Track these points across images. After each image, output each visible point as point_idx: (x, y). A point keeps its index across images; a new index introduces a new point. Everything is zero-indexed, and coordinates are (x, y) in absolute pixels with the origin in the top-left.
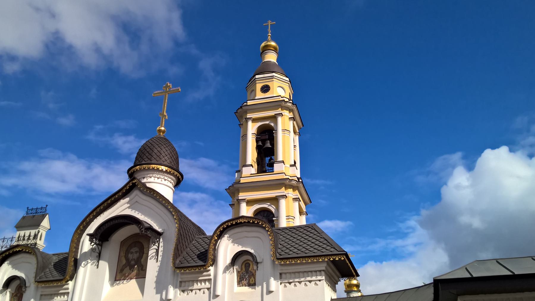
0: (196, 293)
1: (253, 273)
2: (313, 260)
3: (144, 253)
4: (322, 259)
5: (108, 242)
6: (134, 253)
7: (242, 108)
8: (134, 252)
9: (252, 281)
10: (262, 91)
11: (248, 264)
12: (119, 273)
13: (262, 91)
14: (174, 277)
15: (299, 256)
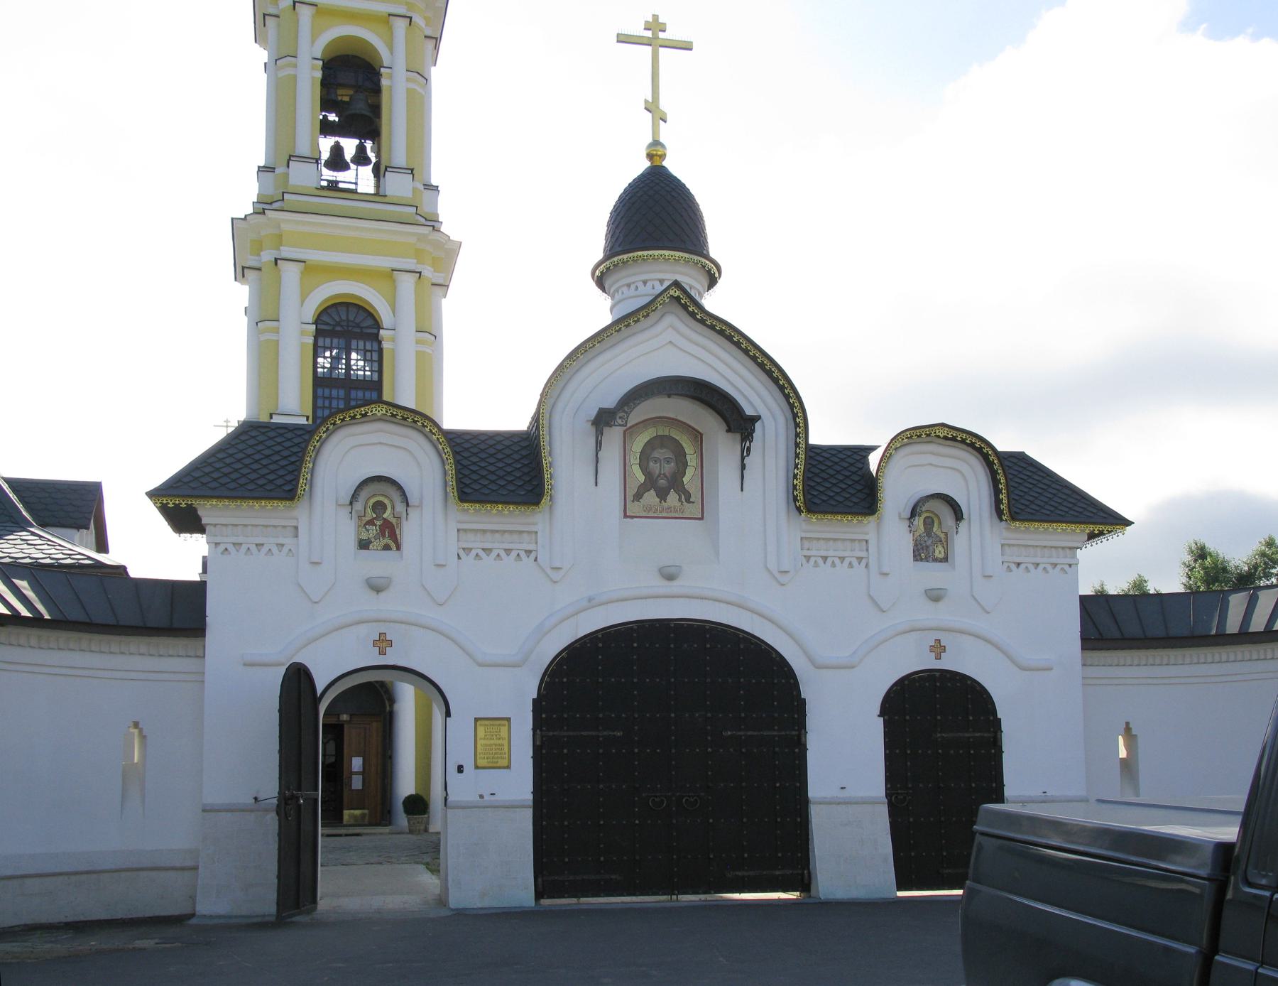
0: (1092, 546)
1: (941, 538)
2: (314, 447)
6: (662, 462)
8: (662, 458)
9: (940, 553)
11: (930, 520)
12: (633, 501)
14: (446, 520)
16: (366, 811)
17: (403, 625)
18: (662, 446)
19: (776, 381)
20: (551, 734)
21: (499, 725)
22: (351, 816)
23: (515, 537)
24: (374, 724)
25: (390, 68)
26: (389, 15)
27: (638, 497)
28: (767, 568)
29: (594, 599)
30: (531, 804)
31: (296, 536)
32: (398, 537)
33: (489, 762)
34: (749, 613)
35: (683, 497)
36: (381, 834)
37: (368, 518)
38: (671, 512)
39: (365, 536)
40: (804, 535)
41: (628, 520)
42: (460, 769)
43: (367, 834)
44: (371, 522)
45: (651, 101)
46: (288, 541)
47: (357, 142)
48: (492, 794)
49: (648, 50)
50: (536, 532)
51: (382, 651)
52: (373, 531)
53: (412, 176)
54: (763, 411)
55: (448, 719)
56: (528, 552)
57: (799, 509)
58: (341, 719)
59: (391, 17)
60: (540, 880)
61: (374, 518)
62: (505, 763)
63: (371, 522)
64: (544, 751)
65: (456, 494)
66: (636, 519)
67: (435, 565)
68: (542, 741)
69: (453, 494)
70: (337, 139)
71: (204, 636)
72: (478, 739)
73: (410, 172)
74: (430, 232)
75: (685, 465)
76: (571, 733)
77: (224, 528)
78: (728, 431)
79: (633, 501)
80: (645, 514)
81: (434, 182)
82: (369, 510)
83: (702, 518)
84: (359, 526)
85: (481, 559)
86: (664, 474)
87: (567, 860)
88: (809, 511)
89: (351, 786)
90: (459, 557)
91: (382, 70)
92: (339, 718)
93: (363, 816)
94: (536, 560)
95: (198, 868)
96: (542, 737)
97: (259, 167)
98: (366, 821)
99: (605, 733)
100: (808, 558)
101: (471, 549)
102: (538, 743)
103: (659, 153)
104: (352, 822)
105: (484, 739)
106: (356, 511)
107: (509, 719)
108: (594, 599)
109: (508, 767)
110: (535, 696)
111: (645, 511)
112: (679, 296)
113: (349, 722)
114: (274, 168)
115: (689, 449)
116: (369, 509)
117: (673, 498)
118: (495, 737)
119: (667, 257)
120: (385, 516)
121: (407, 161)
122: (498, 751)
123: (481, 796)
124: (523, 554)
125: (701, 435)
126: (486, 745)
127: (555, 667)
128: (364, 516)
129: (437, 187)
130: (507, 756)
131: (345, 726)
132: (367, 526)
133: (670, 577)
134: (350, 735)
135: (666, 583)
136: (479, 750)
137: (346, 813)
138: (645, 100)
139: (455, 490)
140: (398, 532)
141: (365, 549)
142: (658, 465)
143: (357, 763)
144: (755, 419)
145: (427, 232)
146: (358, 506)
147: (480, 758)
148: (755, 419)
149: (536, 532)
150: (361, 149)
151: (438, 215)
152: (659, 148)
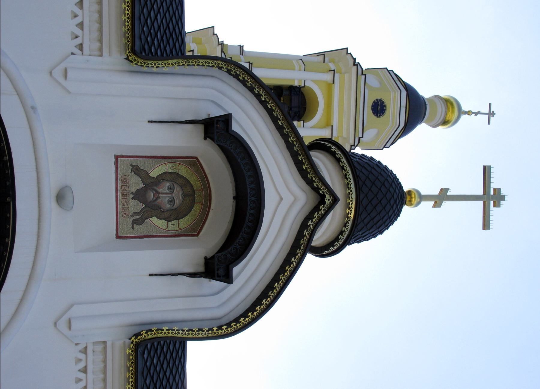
3: (168, 221)
4: (148, 67)
5: (203, 139)
6: (170, 195)
7: (354, 65)
8: (174, 195)
10: (379, 100)
13: (379, 100)
15: (327, 225)
18: (184, 195)
19: (252, 309)
23: (96, 35)
25: (304, 127)
26: (332, 126)
27: (136, 170)
28: (72, 306)
34: (23, 288)
35: (138, 217)
38: (123, 204)
40: (109, 344)
41: (113, 160)
45: (448, 194)
49: (480, 192)
50: (101, 55)
54: (237, 283)
56: (81, 47)
57: (136, 335)
59: (331, 127)
66: (114, 167)
75: (168, 219)
78: (206, 258)
79: (132, 165)
80: (120, 177)
83: (118, 237)
86: (159, 197)
88: (137, 346)
91: (302, 122)
94: (73, 54)
97: (243, 46)
100: (85, 351)
103: (413, 200)
111: (122, 177)
112: (325, 203)
114: (243, 55)
115: (184, 223)
117: (136, 206)
119: (350, 196)
124: (78, 41)
125: (197, 235)
133: (60, 198)
135: (54, 194)
138: (448, 189)
142: (168, 191)
144: (228, 278)
148: (228, 278)
149: (101, 55)
152: (418, 199)
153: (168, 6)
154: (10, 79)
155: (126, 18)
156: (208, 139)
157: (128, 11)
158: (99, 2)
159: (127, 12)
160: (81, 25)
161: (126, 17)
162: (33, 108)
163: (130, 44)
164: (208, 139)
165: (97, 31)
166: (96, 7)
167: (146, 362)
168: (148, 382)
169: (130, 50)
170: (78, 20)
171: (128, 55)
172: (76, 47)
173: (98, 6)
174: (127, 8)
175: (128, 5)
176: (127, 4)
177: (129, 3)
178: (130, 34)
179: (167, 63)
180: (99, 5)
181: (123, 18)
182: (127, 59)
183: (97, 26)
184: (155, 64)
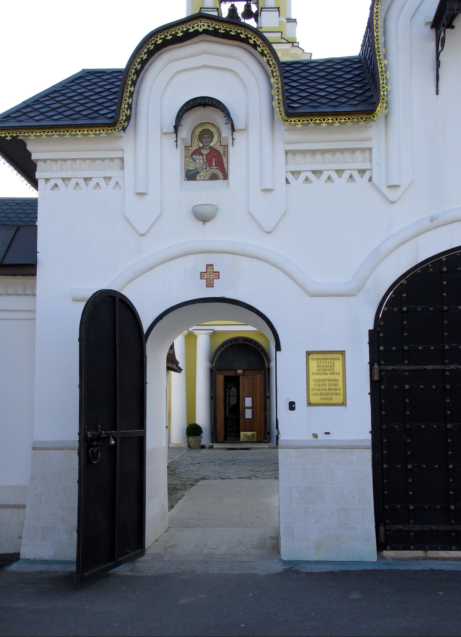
5: (453, 29)
16: (255, 433)
17: (230, 256)
20: (390, 368)
21: (333, 359)
22: (245, 436)
23: (347, 156)
24: (259, 376)
29: (436, 218)
30: (370, 444)
31: (123, 168)
32: (226, 166)
33: (323, 399)
36: (263, 448)
37: (194, 148)
39: (192, 167)
42: (292, 406)
43: (254, 448)
44: (198, 152)
46: (114, 173)
47: (245, 3)
48: (326, 433)
50: (370, 149)
51: (210, 284)
52: (200, 160)
53: (278, 12)
55: (278, 352)
56: (362, 172)
58: (238, 373)
60: (382, 529)
61: (200, 148)
62: (340, 399)
63: (198, 152)
64: (383, 387)
65: (282, 109)
67: (262, 191)
68: (380, 375)
69: (279, 110)
70: (233, 3)
71: (34, 274)
72: (310, 374)
73: (277, 10)
74: (290, 47)
76: (413, 367)
77: (53, 164)
81: (293, 17)
82: (196, 140)
84: (186, 157)
85: (311, 182)
87: (412, 507)
89: (245, 416)
90: (287, 181)
92: (236, 372)
93: (253, 435)
94: (370, 179)
95: (25, 507)
96: (380, 371)
98: (255, 439)
99: (453, 367)
101: (300, 172)
102: (376, 378)
104: (246, 439)
105: (317, 374)
106: (182, 139)
107: (343, 353)
108: (436, 218)
109: (343, 404)
110: (372, 328)
113: (243, 375)
116: (195, 139)
118: (328, 372)
120: (212, 144)
121: (275, 3)
122: (332, 387)
123: (315, 436)
124: (356, 175)
126: (319, 380)
127: (393, 296)
128: (191, 146)
129: (295, 20)
130: (341, 392)
131: (241, 377)
132: (194, 156)
134: (244, 383)
136: (311, 386)
137: (242, 434)
139: (281, 104)
140: (225, 161)
141: (192, 180)
143: (248, 402)
145: (288, 48)
146: (184, 133)
147: (313, 394)
149: (370, 149)
150: (248, 7)
151: (296, 38)
153: (80, 87)
154: (403, 244)
155: (324, 122)
156: (453, 24)
157: (329, 120)
158: (313, 153)
159: (330, 121)
160: (340, 172)
161: (299, 123)
162: (432, 220)
163: (364, 117)
164: (453, 24)
165: (343, 154)
166: (319, 157)
167: (303, 104)
168: (344, 100)
169: (371, 116)
170: (334, 175)
171: (363, 120)
172: (340, 177)
173: (318, 154)
174: (326, 121)
175: (323, 120)
176: (322, 121)
177: (321, 119)
178: (49, 130)
179: (381, 73)
180: (316, 154)
181: (337, 124)
182: (124, 129)
183: (338, 155)
184: (383, 87)
